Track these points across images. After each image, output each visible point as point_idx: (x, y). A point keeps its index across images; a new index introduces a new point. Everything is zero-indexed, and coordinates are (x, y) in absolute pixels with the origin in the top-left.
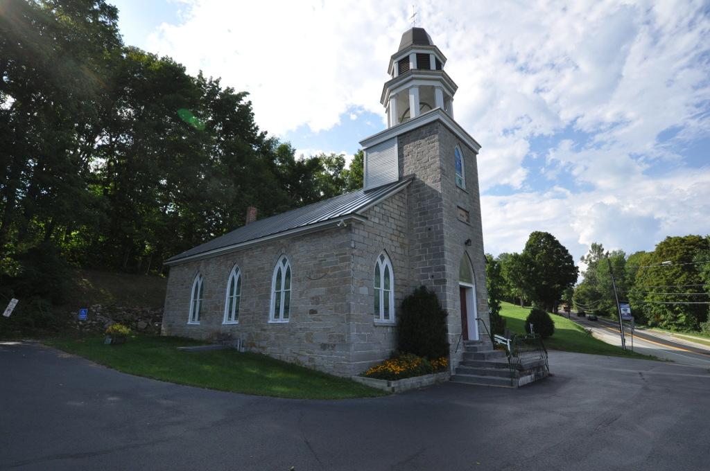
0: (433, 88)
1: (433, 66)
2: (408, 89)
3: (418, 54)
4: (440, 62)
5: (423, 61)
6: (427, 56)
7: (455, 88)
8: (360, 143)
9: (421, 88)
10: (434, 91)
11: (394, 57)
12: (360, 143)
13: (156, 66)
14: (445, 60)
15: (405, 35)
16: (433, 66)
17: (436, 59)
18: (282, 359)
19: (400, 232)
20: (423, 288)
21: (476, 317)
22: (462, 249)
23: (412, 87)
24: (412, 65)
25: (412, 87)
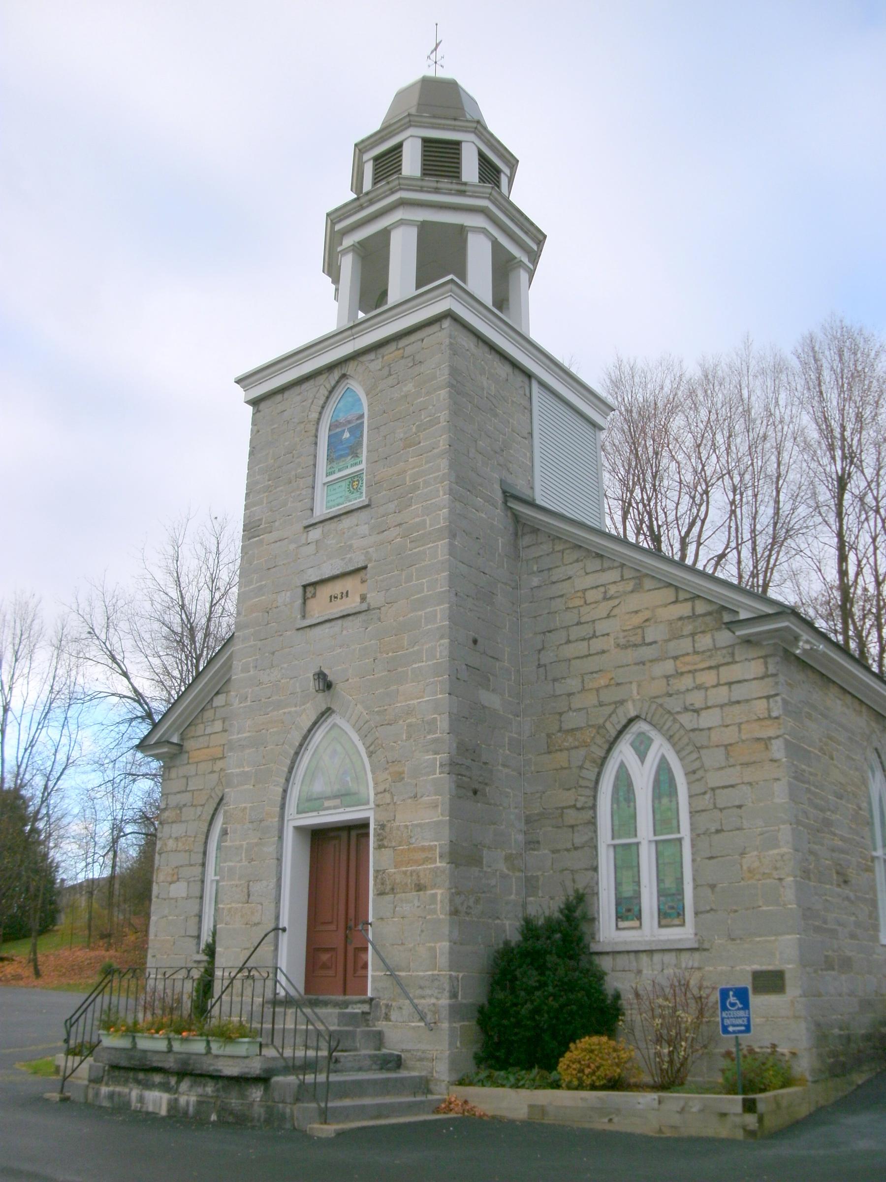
0: (461, 231)
1: (470, 170)
2: (385, 234)
3: (426, 141)
4: (496, 168)
5: (441, 159)
6: (455, 146)
7: (540, 238)
8: (238, 381)
9: (424, 228)
10: (465, 241)
11: (361, 148)
12: (238, 381)
13: (85, 884)
14: (512, 163)
15: (401, 95)
16: (470, 170)
17: (482, 156)
18: (447, 849)
19: (792, 405)
20: (606, 974)
21: (284, 939)
22: (189, 745)
23: (402, 222)
24: (411, 163)
25: (402, 222)
